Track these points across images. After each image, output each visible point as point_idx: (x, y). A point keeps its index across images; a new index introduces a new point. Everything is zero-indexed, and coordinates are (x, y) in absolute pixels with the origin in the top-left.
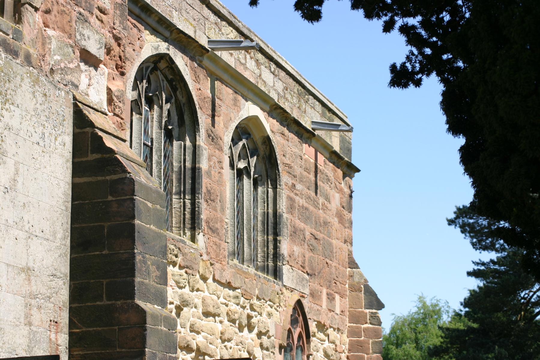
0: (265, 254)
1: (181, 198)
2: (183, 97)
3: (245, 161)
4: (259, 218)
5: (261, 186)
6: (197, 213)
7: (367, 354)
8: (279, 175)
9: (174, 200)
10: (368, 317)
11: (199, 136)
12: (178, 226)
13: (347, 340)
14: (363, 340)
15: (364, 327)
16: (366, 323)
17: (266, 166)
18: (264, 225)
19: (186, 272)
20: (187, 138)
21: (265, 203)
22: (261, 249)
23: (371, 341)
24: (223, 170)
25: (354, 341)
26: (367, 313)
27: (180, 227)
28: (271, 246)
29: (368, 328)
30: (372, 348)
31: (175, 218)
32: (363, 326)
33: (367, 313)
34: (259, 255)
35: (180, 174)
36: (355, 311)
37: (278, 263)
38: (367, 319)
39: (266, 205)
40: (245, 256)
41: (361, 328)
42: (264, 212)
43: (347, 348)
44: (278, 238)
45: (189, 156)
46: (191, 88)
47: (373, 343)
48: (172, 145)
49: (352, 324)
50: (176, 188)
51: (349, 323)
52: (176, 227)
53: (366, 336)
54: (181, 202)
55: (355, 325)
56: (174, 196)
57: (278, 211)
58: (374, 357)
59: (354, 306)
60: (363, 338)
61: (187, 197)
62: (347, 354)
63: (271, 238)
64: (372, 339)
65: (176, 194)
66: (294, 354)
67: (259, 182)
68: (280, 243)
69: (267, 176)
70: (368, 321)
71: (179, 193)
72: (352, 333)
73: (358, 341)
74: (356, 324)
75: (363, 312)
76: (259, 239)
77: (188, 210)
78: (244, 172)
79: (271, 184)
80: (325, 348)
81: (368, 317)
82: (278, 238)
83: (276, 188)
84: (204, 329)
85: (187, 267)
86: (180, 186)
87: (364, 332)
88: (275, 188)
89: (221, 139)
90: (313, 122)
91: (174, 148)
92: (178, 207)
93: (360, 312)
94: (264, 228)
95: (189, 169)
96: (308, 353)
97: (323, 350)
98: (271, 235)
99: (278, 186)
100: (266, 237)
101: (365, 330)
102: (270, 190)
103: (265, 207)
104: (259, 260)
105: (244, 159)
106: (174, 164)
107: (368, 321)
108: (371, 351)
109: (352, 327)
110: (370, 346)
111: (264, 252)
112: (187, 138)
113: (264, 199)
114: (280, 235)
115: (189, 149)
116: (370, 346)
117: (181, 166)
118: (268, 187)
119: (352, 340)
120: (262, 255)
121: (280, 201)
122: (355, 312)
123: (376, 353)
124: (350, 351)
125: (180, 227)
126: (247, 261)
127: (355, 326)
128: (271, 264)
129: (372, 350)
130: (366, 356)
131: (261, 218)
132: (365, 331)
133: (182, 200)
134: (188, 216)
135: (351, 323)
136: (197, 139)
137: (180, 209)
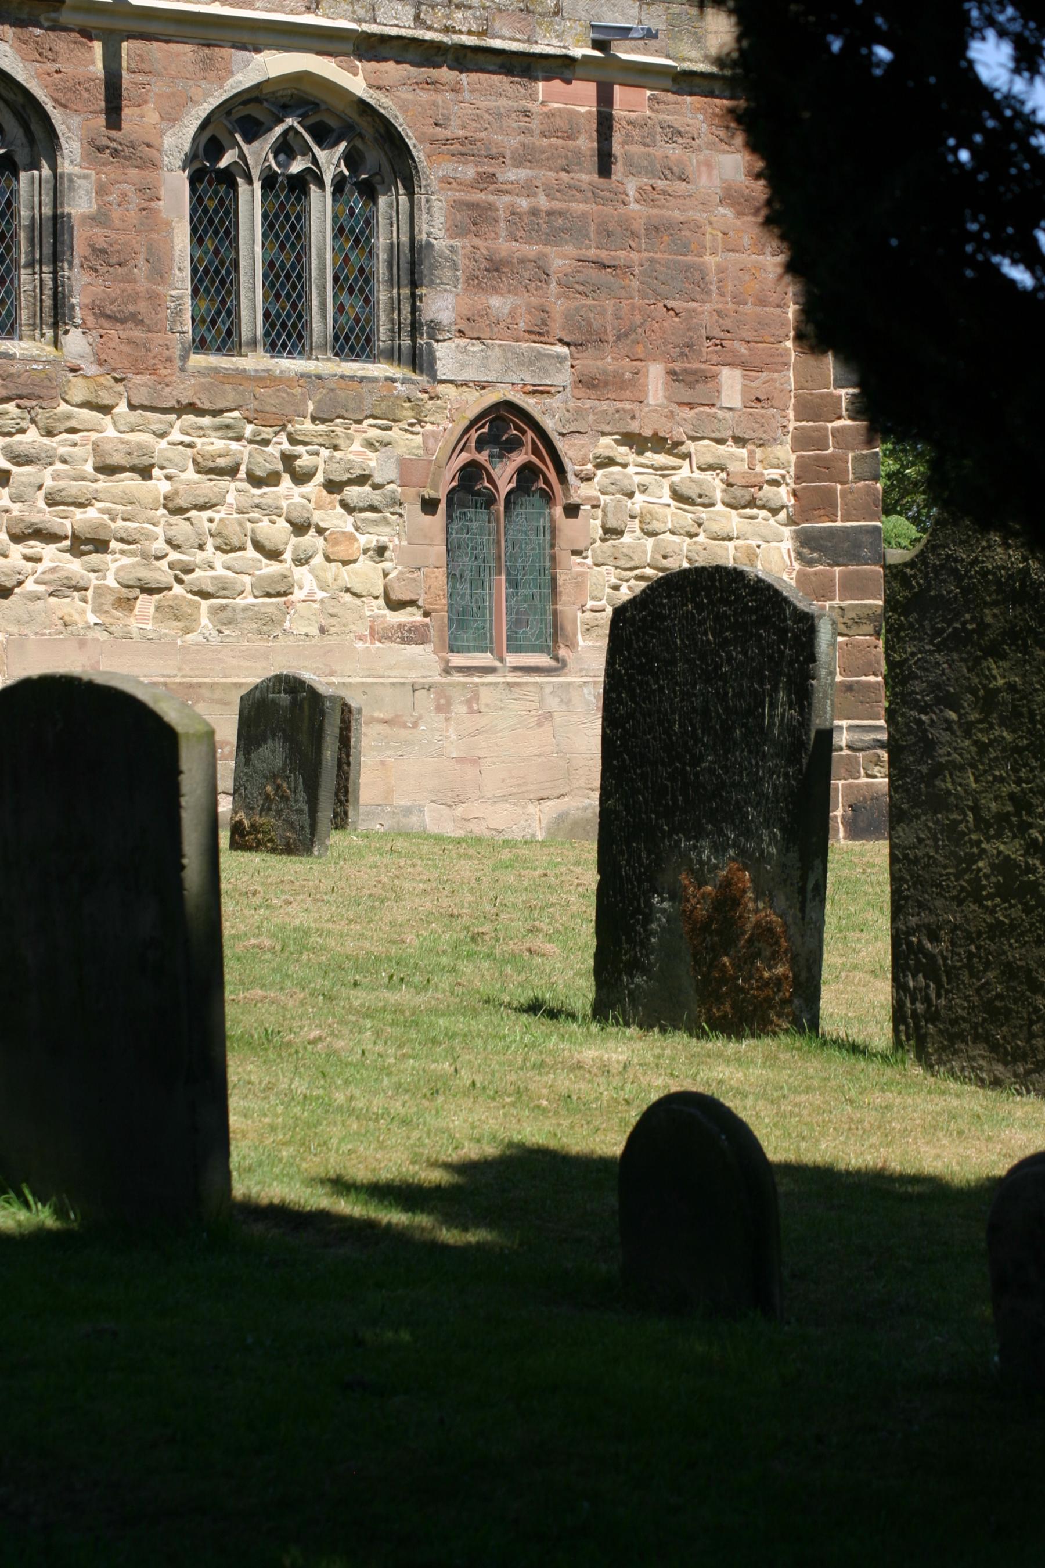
0: (393, 324)
1: (34, 273)
2: (15, 95)
3: (306, 158)
4: (381, 257)
5: (384, 194)
6: (60, 295)
7: (842, 483)
8: (416, 167)
9: (23, 277)
10: (844, 405)
11: (62, 156)
12: (31, 322)
13: (793, 458)
14: (832, 455)
15: (833, 428)
16: (839, 418)
17: (386, 153)
18: (392, 270)
19: (18, 406)
20: (44, 163)
21: (392, 226)
22: (387, 316)
23: (851, 455)
24: (161, 203)
25: (809, 457)
26: (840, 397)
27: (34, 324)
28: (406, 309)
29: (844, 427)
30: (853, 469)
31: (27, 308)
32: (830, 425)
33: (840, 397)
34: (381, 329)
35: (33, 230)
36: (812, 394)
37: (419, 341)
38: (841, 408)
39: (395, 229)
40: (314, 339)
41: (827, 429)
42: (392, 244)
43: (792, 473)
44: (418, 292)
45: (47, 195)
46: (20, 78)
47: (855, 459)
48: (17, 179)
49: (804, 423)
50: (26, 256)
51: (796, 420)
52: (29, 325)
53: (837, 445)
54: (34, 280)
55: (811, 424)
56: (23, 271)
57: (417, 238)
58: (860, 488)
59: (809, 385)
60: (831, 450)
61: (45, 269)
62: (793, 485)
63: (406, 291)
64: (853, 450)
65: (26, 267)
66: (498, 511)
67: (378, 187)
68: (421, 301)
69: (395, 173)
70: (844, 413)
71: (31, 264)
72: (802, 441)
73: (818, 458)
74: (814, 422)
75: (830, 395)
76: (381, 297)
77: (48, 292)
78: (308, 178)
79: (403, 185)
80: (673, 483)
81: (844, 405)
82: (418, 292)
83: (414, 193)
84: (101, 496)
85: (21, 397)
86: (33, 252)
87: (833, 436)
88: (410, 193)
89: (148, 145)
90: (593, 26)
91: (22, 185)
92: (31, 288)
93: (822, 396)
94: (392, 275)
95: (48, 218)
96: (565, 502)
97: (670, 487)
98: (406, 286)
99: (417, 190)
100: (395, 291)
101: (836, 432)
102: (403, 199)
103: (392, 233)
104: (382, 338)
105: (303, 155)
106: (22, 213)
107: (844, 413)
108: (851, 476)
109: (802, 428)
110: (850, 465)
111: (392, 321)
112: (44, 163)
113: (391, 217)
114: (421, 286)
115: (47, 182)
116: (850, 465)
117: (33, 216)
118: (397, 194)
119: (803, 456)
120: (389, 326)
121: (420, 218)
122: (810, 397)
123: (865, 480)
124: (798, 479)
125: (34, 324)
126: (318, 347)
127: (811, 427)
128: (406, 342)
129: (854, 474)
130: (839, 487)
131: (385, 257)
132: (837, 434)
133: (37, 276)
134: (48, 302)
135: (801, 421)
136: (59, 162)
137: (34, 291)
